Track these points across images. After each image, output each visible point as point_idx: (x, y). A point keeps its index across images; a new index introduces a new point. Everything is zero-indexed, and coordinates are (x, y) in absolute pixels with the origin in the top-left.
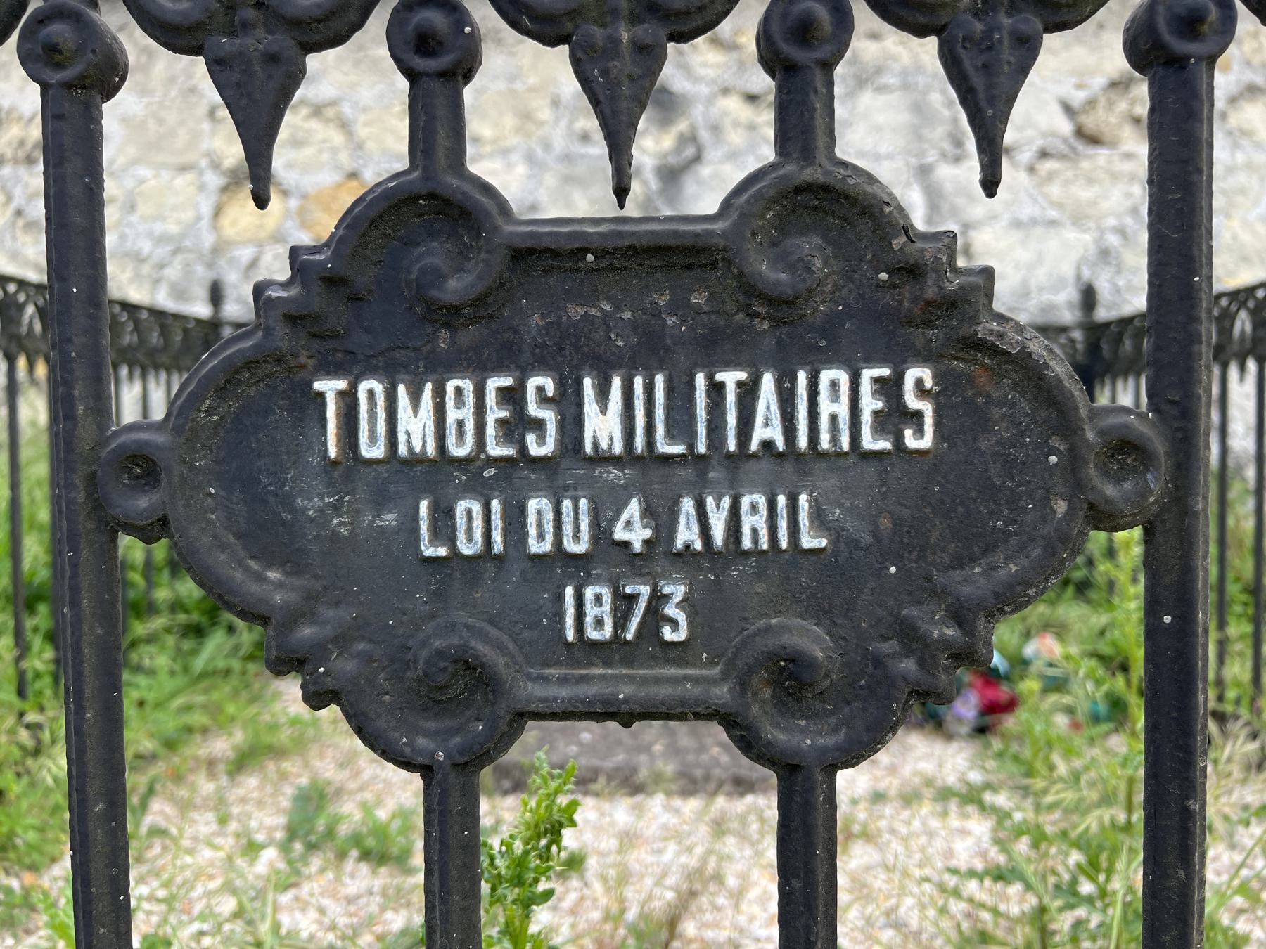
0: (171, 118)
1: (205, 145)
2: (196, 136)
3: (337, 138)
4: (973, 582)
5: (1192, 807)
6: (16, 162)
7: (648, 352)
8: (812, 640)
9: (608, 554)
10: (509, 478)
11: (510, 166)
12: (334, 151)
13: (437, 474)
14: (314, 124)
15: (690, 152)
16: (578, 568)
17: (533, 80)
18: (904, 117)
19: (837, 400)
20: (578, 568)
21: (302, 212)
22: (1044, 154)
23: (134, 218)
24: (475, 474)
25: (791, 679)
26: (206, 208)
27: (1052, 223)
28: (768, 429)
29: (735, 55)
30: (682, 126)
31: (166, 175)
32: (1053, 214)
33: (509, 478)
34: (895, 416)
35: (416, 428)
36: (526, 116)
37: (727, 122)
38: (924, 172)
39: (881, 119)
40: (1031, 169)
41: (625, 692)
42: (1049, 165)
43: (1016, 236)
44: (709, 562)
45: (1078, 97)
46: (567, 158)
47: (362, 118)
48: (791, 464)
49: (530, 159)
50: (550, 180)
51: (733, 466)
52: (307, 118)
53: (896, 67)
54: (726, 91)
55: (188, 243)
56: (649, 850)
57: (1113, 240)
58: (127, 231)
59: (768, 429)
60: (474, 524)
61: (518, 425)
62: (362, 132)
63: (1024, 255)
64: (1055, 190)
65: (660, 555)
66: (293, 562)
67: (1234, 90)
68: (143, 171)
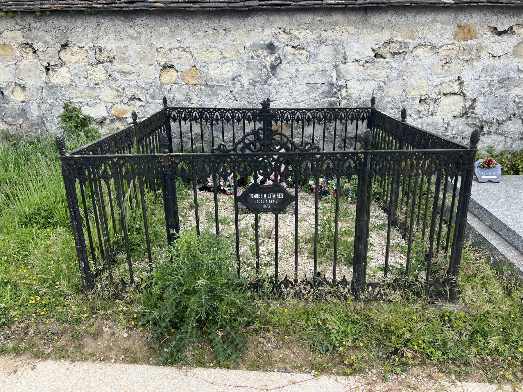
0: (147, 51)
1: (156, 59)
2: (154, 56)
3: (190, 57)
4: (285, 204)
5: (372, 208)
6: (107, 61)
7: (267, 193)
8: (277, 207)
9: (265, 203)
10: (260, 199)
11: (233, 64)
12: (189, 60)
13: (256, 199)
14: (183, 53)
15: (279, 61)
16: (264, 204)
17: (238, 42)
18: (332, 52)
19: (278, 195)
20: (264, 204)
21: (181, 76)
22: (366, 62)
23: (139, 78)
24: (258, 199)
25: (275, 209)
26: (158, 76)
27: (368, 80)
28: (274, 197)
29: (290, 35)
30: (277, 54)
31: (147, 66)
32: (368, 77)
33: (260, 199)
34: (281, 196)
35: (255, 196)
36: (237, 52)
37: (288, 54)
38: (336, 66)
39: (326, 53)
40: (363, 66)
41: (266, 211)
42: (368, 64)
43: (359, 83)
44: (271, 204)
45: (376, 47)
46: (248, 63)
47: (195, 52)
48: (275, 199)
49: (238, 63)
50: (244, 68)
51: (272, 199)
52: (181, 51)
53: (331, 39)
54: (287, 45)
55: (153, 84)
56: (508, 387)
57: (382, 84)
58: (138, 81)
59: (274, 197)
60: (258, 201)
61: (260, 196)
62: (196, 56)
63: (360, 88)
64: (368, 71)
65: (268, 203)
66: (248, 203)
67: (415, 45)
68: (141, 65)
